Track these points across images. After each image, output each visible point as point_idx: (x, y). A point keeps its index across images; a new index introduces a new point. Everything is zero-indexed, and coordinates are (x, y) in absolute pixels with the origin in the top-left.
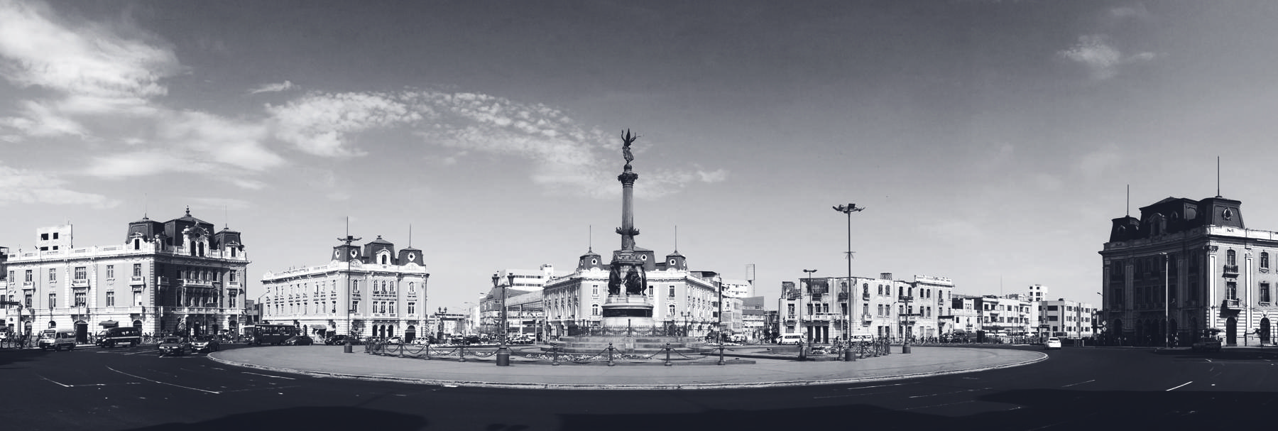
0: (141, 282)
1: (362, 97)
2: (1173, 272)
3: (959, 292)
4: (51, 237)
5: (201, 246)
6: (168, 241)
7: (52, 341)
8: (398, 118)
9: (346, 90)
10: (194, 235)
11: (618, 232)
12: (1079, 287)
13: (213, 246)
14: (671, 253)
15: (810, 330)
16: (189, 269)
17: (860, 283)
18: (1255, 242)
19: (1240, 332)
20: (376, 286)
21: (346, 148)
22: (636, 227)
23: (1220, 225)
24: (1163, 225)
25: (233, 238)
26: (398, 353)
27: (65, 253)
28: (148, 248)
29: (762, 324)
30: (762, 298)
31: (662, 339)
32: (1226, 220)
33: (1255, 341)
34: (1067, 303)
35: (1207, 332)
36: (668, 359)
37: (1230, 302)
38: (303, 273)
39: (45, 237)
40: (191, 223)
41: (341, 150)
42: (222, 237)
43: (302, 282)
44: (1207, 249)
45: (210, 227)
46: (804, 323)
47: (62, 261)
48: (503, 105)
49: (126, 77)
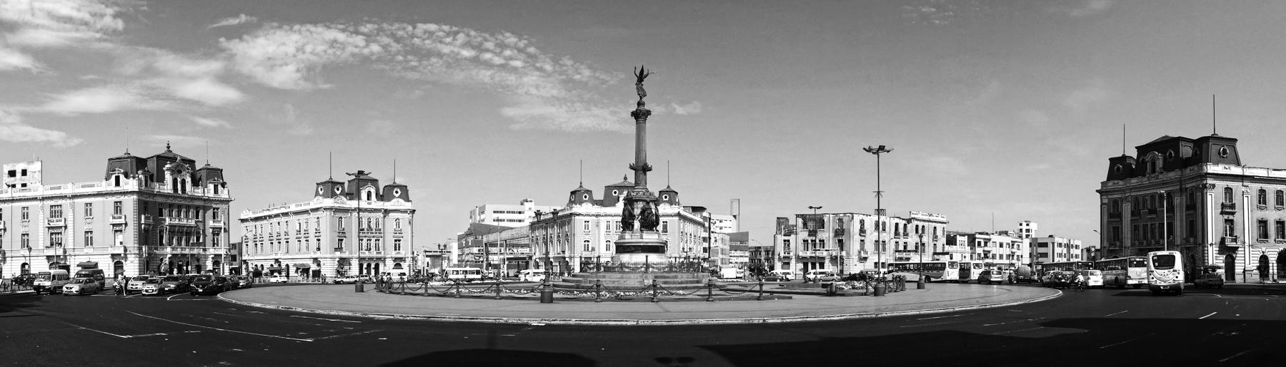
0: (122, 221)
1: (320, 29)
2: (1171, 209)
3: (952, 228)
4: (19, 174)
5: (183, 182)
6: (150, 178)
7: (48, 284)
8: (356, 50)
9: (303, 22)
10: (176, 171)
11: (631, 168)
12: (1075, 225)
13: (196, 183)
14: (664, 188)
15: (806, 265)
16: (171, 206)
17: (857, 218)
18: (1252, 179)
19: (1239, 269)
20: (360, 223)
21: (306, 79)
22: (649, 164)
23: (1217, 163)
24: (1160, 163)
25: (215, 175)
26: (422, 291)
27: (41, 191)
28: (131, 184)
29: (747, 260)
30: (747, 234)
31: (679, 275)
32: (1222, 158)
33: (1255, 278)
34: (1057, 240)
35: (1206, 270)
36: (710, 294)
37: (1228, 238)
38: (284, 210)
39: (12, 174)
40: (173, 159)
41: (301, 82)
42: (204, 174)
43: (283, 219)
44: (1205, 186)
45: (192, 162)
46: (799, 259)
47: (35, 199)
48: (468, 35)
49: (79, 10)
